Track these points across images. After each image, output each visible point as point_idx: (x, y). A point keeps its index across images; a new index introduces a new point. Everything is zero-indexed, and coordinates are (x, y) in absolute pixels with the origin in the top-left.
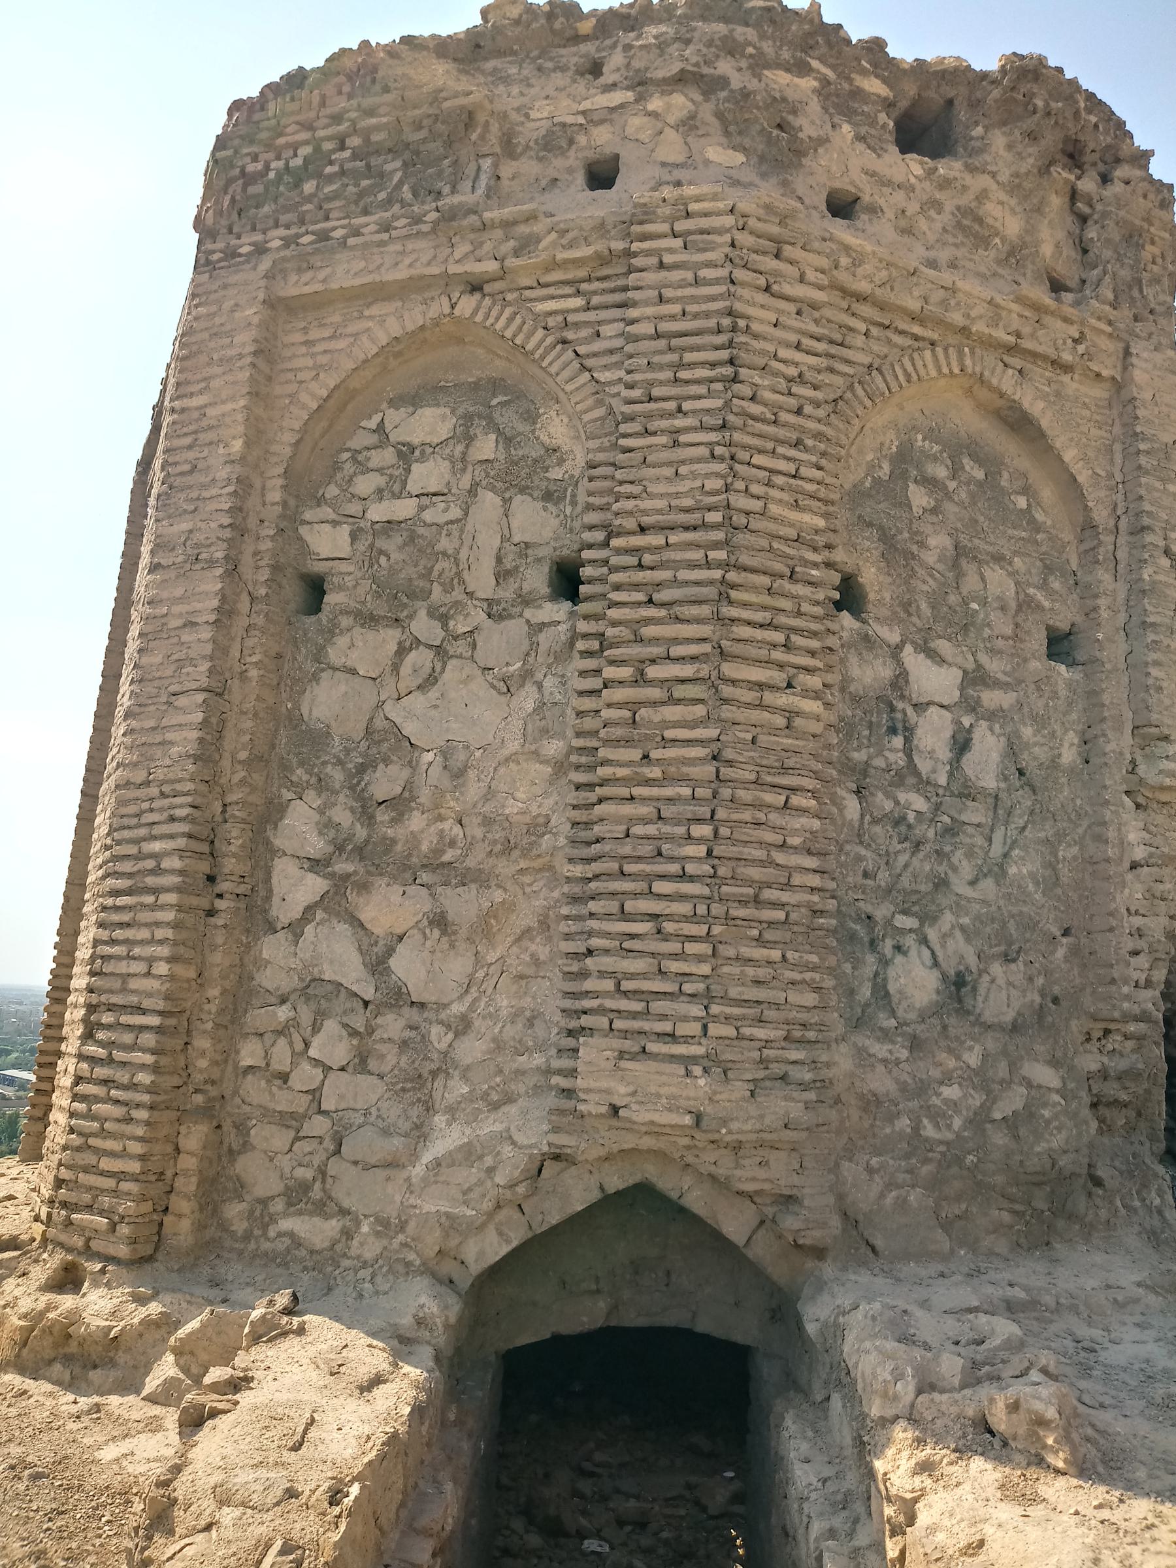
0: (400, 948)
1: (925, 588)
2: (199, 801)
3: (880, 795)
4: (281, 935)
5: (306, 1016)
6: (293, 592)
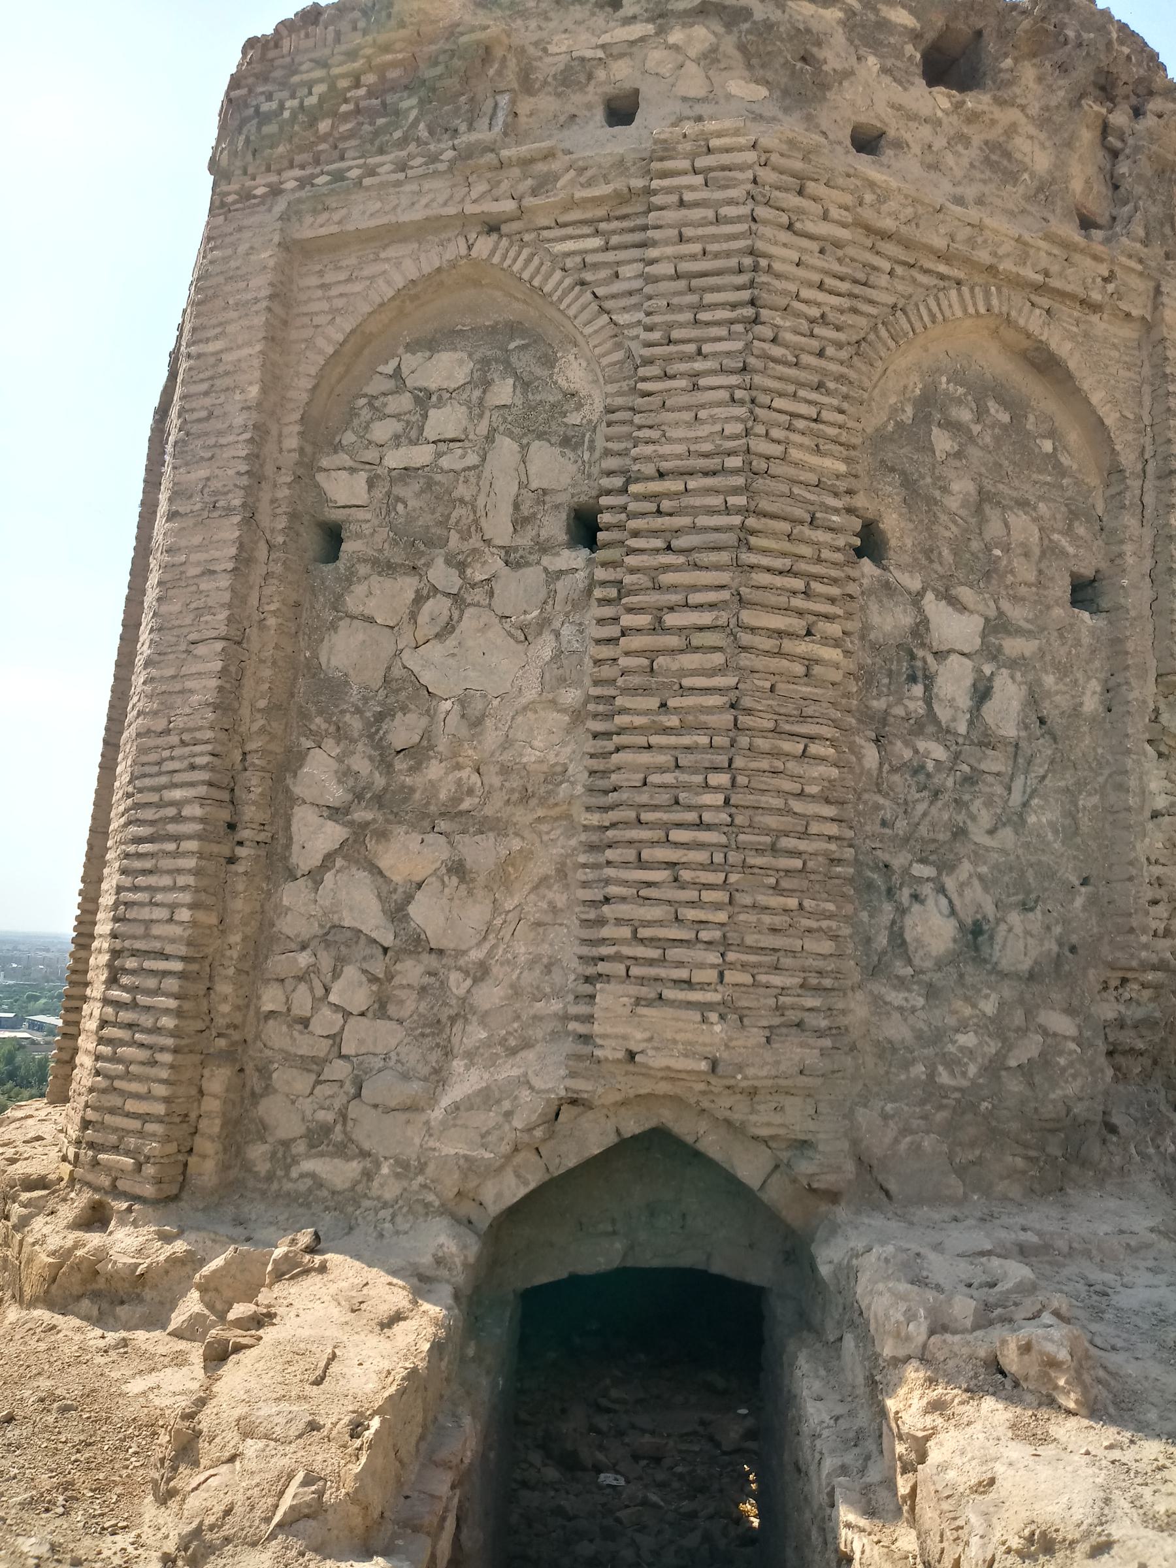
0: (419, 896)
1: (947, 534)
2: (219, 749)
3: (899, 744)
4: (301, 882)
6: (311, 540)
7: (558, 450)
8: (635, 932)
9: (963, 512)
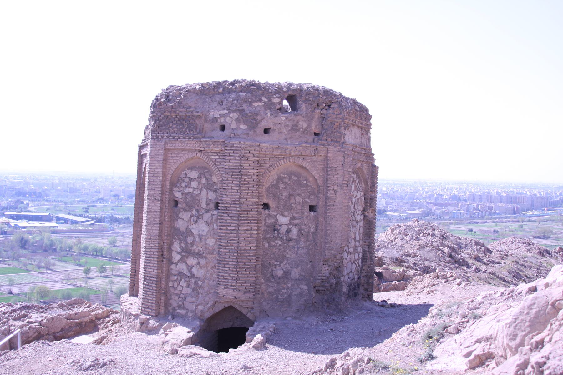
5: (179, 279)
6: (173, 204)
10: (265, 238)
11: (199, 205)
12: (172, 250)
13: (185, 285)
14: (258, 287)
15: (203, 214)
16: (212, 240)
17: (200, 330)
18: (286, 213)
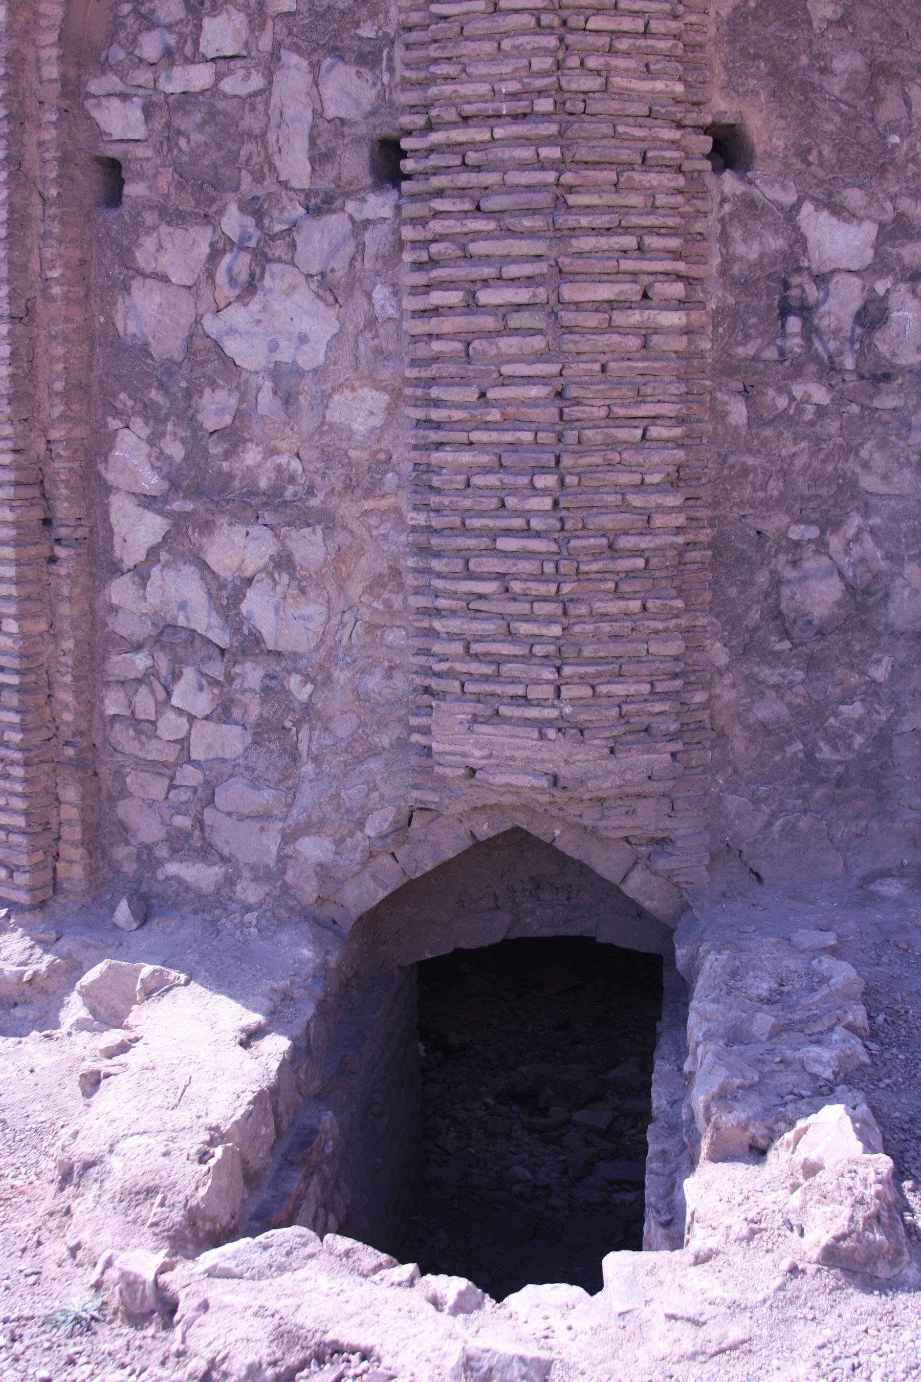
0: (250, 593)
1: (830, 128)
2: (21, 445)
3: (771, 393)
4: (127, 578)
5: (164, 666)
6: (89, 183)
7: (352, 70)
8: (467, 648)
9: (849, 97)
10: (728, 368)
11: (266, 168)
12: (108, 489)
13: (202, 703)
14: (699, 697)
15: (294, 225)
16: (368, 393)
17: (321, 1005)
18: (854, 197)
